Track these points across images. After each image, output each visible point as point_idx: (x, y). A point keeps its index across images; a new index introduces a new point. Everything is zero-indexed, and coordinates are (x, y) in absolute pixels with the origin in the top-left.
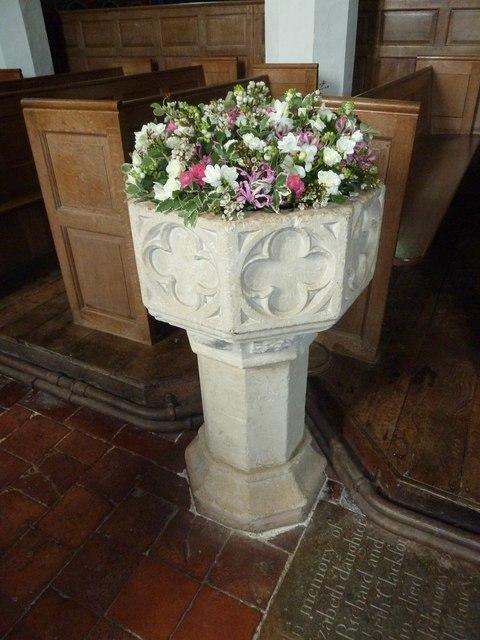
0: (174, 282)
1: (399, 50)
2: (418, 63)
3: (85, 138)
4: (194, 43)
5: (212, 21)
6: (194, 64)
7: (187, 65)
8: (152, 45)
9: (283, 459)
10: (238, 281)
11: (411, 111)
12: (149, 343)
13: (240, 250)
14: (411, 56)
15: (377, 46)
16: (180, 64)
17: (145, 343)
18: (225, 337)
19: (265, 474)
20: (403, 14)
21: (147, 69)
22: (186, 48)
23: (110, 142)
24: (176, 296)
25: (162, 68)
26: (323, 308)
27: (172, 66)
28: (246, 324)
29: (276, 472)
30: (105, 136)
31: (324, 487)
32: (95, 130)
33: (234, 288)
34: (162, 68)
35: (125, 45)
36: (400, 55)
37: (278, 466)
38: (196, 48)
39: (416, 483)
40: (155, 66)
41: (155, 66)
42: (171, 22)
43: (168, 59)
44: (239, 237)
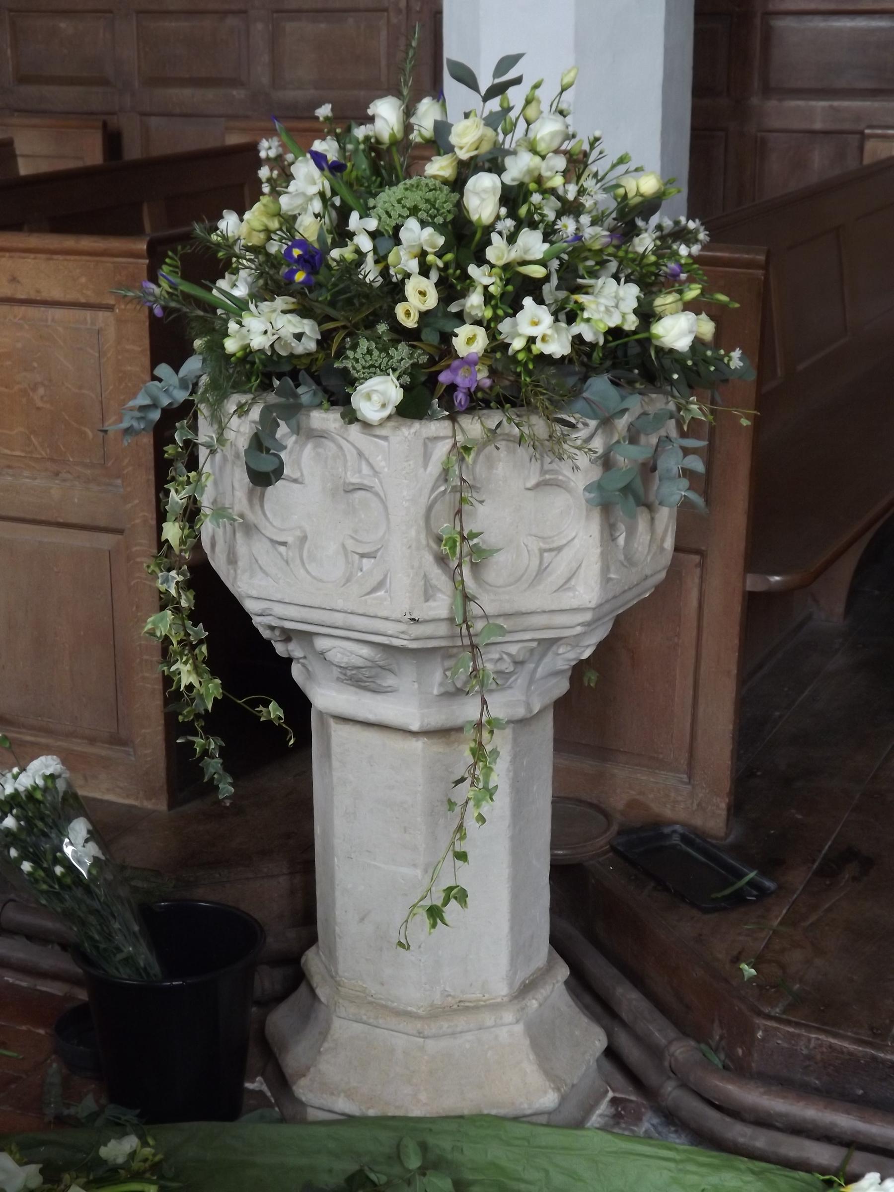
0: (304, 539)
1: (818, 112)
2: (869, 145)
3: (59, 313)
4: (234, 82)
5: (290, 26)
6: (234, 139)
7: (211, 143)
8: (104, 82)
9: (501, 989)
10: (422, 523)
11: (749, 265)
12: (159, 805)
13: (425, 466)
14: (847, 126)
15: (755, 101)
16: (192, 138)
17: (148, 805)
18: (538, 93)
19: (461, 1022)
20: (820, 23)
21: (91, 153)
22: (210, 94)
23: (120, 321)
24: (303, 564)
25: (133, 151)
26: (565, 586)
27: (162, 148)
28: (431, 603)
29: (489, 1019)
30: (110, 308)
31: (604, 1107)
32: (89, 295)
33: (413, 533)
34: (133, 151)
35: (23, 79)
36: (818, 126)
37: (495, 1007)
38: (238, 94)
39: (797, 1025)
40: (113, 142)
41: (113, 142)
42: (170, 24)
43: (154, 121)
44: (425, 445)
